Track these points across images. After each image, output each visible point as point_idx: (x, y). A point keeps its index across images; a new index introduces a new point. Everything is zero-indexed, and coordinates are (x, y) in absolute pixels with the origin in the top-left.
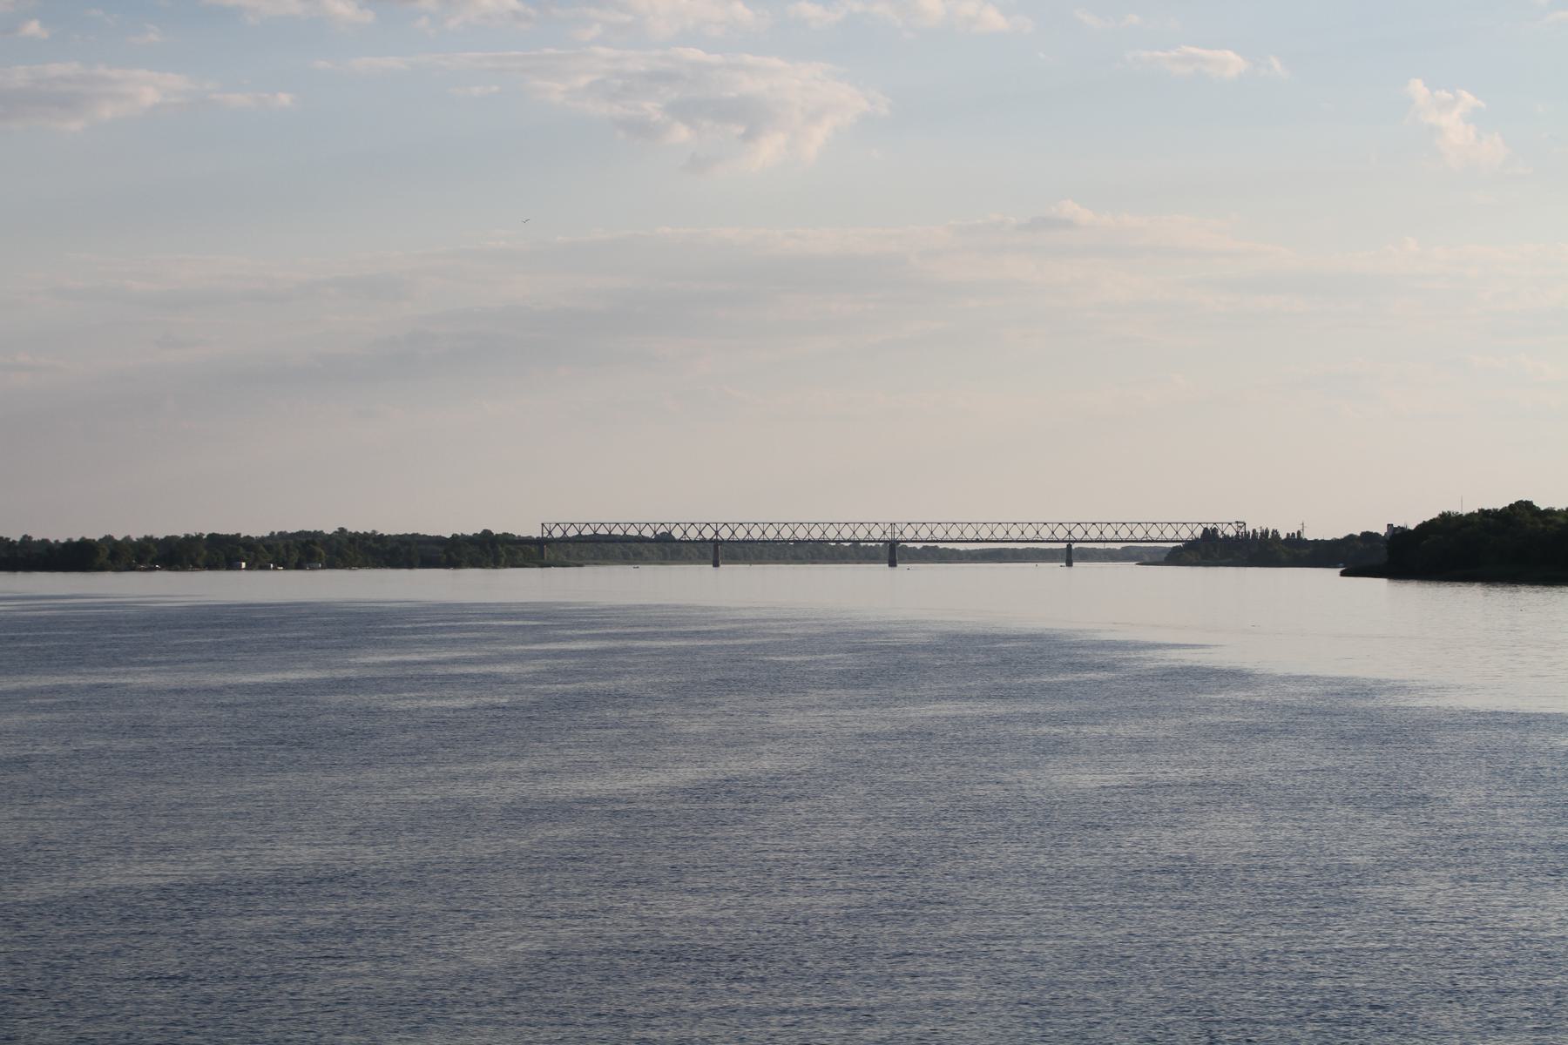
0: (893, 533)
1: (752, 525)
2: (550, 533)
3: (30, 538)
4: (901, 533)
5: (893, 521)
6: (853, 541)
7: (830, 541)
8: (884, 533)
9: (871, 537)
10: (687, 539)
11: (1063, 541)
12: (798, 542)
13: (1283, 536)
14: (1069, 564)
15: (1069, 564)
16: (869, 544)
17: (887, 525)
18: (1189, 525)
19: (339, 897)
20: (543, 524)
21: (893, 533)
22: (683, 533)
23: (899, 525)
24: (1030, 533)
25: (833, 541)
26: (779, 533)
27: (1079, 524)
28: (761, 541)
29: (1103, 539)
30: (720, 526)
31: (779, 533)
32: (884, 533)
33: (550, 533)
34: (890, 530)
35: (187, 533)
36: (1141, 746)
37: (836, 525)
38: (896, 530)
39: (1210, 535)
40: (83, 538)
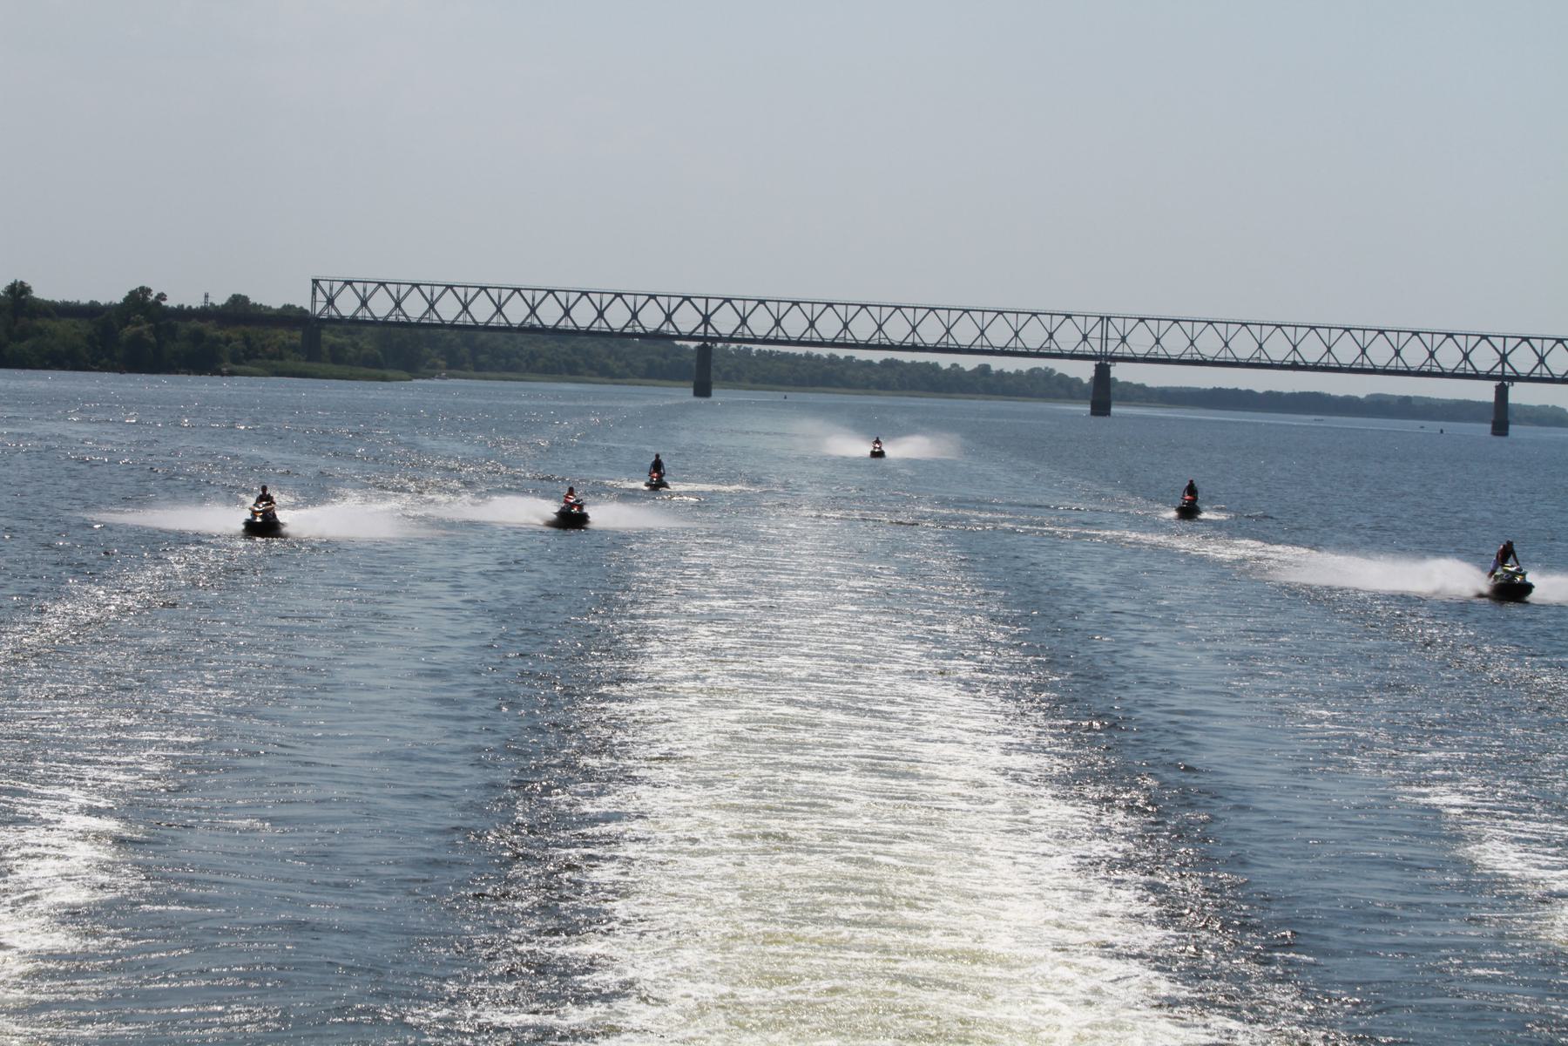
0: (1105, 338)
1: (923, 312)
2: (330, 301)
3: (245, 299)
4: (1123, 339)
5: (1105, 312)
6: (705, 338)
7: (680, 337)
8: (1085, 338)
9: (1161, 352)
10: (402, 318)
11: (1488, 377)
12: (353, 324)
13: (186, 307)
14: (703, 390)
15: (703, 390)
16: (815, 351)
17: (1092, 321)
18: (1356, 333)
19: (842, 1034)
20: (316, 282)
21: (1105, 338)
22: (629, 316)
23: (663, 301)
24: (897, 330)
25: (690, 337)
26: (948, 331)
27: (1069, 316)
28: (459, 327)
29: (816, 337)
30: (713, 304)
31: (948, 331)
32: (1085, 338)
33: (330, 301)
34: (1097, 332)
35: (29, 282)
36: (1316, 889)
37: (909, 313)
38: (1112, 333)
39: (140, 304)
40: (92, 302)
